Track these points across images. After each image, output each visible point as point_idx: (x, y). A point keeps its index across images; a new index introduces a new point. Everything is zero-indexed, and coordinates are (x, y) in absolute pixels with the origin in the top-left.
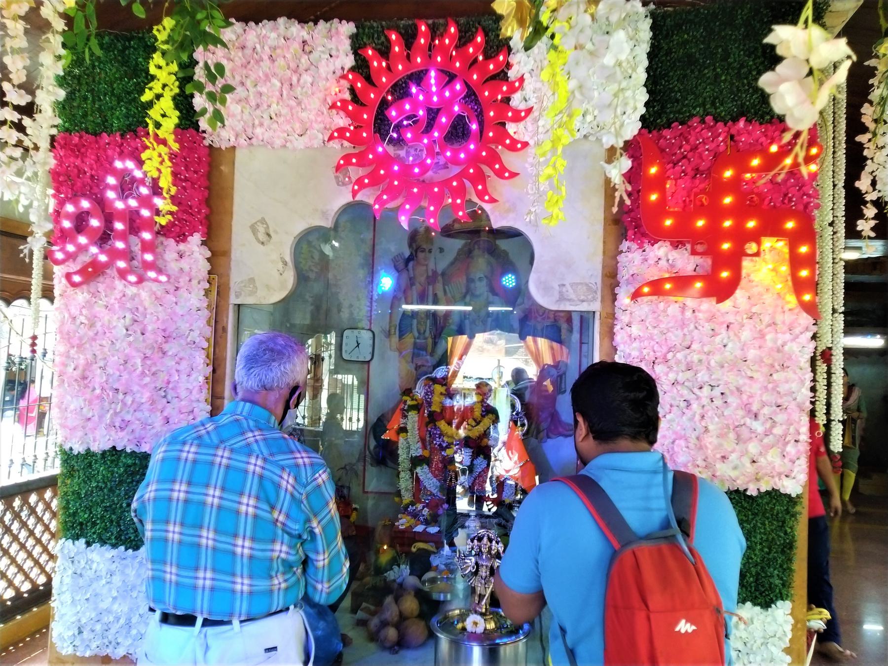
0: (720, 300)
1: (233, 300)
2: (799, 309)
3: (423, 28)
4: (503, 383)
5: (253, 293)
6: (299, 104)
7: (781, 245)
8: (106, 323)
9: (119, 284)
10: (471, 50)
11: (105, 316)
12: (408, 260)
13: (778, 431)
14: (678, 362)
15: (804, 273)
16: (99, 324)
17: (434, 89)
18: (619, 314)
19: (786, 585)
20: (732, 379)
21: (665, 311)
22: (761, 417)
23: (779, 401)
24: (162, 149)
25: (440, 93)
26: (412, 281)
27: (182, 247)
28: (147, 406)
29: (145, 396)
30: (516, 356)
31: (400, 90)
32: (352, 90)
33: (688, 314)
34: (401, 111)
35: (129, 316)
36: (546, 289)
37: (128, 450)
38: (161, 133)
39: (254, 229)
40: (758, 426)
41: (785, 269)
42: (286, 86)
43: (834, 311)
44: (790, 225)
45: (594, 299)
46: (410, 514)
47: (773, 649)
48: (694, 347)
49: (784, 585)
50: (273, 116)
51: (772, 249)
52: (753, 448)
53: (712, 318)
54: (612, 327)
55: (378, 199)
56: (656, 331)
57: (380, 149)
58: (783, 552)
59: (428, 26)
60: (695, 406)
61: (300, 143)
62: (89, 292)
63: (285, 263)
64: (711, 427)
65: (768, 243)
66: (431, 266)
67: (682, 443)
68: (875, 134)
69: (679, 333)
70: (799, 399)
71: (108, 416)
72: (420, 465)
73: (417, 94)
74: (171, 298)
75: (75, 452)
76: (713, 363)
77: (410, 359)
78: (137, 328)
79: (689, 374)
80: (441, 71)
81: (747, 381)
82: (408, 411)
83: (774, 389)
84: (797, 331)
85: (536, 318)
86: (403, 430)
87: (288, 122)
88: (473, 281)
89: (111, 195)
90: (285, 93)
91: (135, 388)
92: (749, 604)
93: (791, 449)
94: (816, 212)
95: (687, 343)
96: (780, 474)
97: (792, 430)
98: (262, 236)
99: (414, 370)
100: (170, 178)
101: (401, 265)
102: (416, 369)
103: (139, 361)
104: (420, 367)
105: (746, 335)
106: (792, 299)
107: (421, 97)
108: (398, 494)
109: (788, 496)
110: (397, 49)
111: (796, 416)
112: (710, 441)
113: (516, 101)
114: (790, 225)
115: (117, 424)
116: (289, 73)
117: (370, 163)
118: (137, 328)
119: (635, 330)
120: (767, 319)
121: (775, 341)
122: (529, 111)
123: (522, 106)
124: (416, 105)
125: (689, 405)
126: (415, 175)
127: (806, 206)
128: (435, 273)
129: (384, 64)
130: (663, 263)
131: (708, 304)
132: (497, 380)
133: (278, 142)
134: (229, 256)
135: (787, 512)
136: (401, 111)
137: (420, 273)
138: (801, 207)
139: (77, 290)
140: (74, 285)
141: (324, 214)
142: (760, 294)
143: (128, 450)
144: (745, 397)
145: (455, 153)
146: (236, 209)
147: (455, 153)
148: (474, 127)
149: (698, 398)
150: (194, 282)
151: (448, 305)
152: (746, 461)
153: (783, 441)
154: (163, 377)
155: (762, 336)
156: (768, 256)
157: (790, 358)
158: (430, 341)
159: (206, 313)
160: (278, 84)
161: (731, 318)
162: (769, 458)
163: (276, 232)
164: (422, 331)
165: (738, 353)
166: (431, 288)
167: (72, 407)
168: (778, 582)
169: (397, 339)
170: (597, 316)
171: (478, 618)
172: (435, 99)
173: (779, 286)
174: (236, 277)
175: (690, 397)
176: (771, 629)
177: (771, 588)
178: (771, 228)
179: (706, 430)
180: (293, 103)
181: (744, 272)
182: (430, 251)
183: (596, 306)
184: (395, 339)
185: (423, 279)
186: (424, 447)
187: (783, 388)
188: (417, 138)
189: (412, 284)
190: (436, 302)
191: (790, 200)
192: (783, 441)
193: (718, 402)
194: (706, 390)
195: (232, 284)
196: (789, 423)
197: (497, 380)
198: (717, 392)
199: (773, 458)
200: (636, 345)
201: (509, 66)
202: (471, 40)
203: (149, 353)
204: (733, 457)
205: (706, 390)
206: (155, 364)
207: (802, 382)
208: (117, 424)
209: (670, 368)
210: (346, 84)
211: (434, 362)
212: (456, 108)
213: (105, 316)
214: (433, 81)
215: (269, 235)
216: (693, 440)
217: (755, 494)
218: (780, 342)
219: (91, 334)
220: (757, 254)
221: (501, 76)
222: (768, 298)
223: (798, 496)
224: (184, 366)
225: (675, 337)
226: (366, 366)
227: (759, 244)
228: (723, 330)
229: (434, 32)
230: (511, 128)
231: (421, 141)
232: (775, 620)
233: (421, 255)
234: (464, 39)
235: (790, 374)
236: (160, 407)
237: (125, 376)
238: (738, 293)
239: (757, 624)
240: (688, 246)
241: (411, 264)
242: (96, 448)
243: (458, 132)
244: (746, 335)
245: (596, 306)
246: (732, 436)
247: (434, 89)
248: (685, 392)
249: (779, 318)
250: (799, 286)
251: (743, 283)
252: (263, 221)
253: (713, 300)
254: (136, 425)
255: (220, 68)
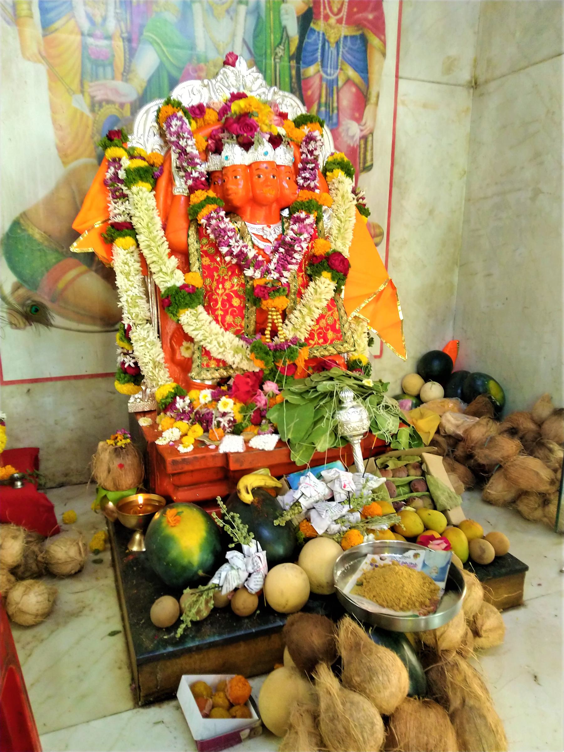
46: (182, 415)
72: (189, 305)
77: (75, 85)
82: (128, 182)
85: (327, 18)
86: (126, 228)
99: (87, 111)
102: (93, 110)
104: (100, 104)
108: (135, 375)
146: (36, 716)
158: (119, 45)
164: (98, 20)
169: (39, 31)
186: (186, 267)
211: (133, 96)
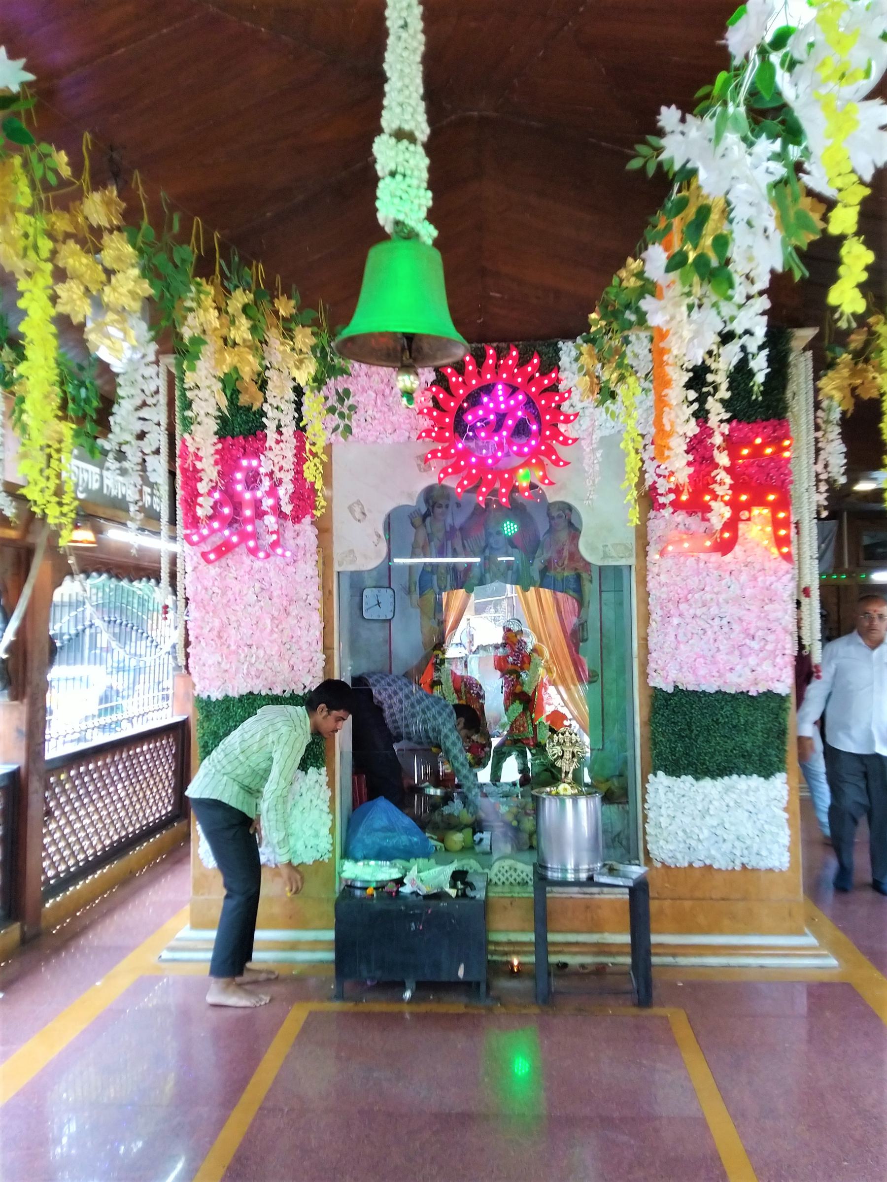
0: (724, 554)
1: (337, 568)
2: (780, 559)
3: (491, 352)
4: (474, 649)
5: (353, 561)
6: (390, 410)
7: (766, 512)
8: (237, 591)
9: (247, 560)
10: (530, 369)
11: (236, 586)
12: (424, 517)
13: (769, 647)
14: (696, 601)
15: (782, 532)
16: (230, 593)
17: (501, 399)
18: (650, 566)
19: (782, 761)
20: (732, 611)
21: (684, 563)
22: (757, 638)
23: (770, 626)
24: (317, 460)
25: (506, 401)
26: (430, 537)
27: (297, 527)
28: (276, 657)
29: (274, 650)
30: (485, 615)
31: (474, 399)
32: (435, 399)
33: (702, 565)
34: (475, 416)
35: (258, 585)
36: (592, 549)
37: (263, 693)
38: (314, 449)
39: (351, 509)
40: (755, 645)
41: (769, 529)
42: (380, 396)
43: (811, 557)
44: (771, 497)
45: (630, 556)
47: (775, 809)
48: (707, 589)
49: (780, 761)
50: (369, 419)
51: (760, 514)
52: (752, 661)
53: (718, 568)
54: (645, 576)
55: (460, 485)
56: (679, 579)
57: (460, 446)
58: (778, 737)
59: (494, 349)
60: (709, 632)
61: (389, 440)
62: (220, 567)
63: (379, 536)
64: (721, 648)
65: (756, 511)
66: (449, 520)
67: (702, 660)
68: (825, 432)
69: (696, 579)
70: (784, 623)
71: (245, 667)
73: (488, 403)
74: (291, 569)
75: (214, 699)
76: (721, 600)
77: (432, 616)
78: (266, 595)
79: (704, 609)
80: (506, 385)
81: (745, 612)
83: (765, 617)
84: (780, 574)
85: (555, 569)
87: (380, 424)
88: (491, 534)
89: (239, 487)
90: (379, 402)
91: (266, 643)
92: (755, 776)
93: (779, 660)
94: (791, 487)
95: (702, 587)
96: (772, 679)
97: (779, 646)
98: (358, 515)
100: (321, 482)
101: (418, 521)
103: (268, 622)
105: (744, 578)
106: (774, 550)
107: (491, 405)
109: (779, 695)
110: (470, 368)
111: (782, 636)
112: (721, 657)
113: (565, 407)
114: (771, 497)
115: (253, 673)
116: (382, 386)
117: (453, 456)
118: (266, 595)
119: (663, 578)
120: (758, 566)
121: (764, 582)
122: (576, 415)
123: (570, 411)
124: (488, 411)
125: (705, 633)
126: (489, 465)
127: (783, 481)
128: (452, 527)
129: (460, 379)
130: (681, 527)
131: (716, 557)
132: (467, 645)
133: (371, 439)
134: (331, 533)
135: (780, 707)
136: (475, 416)
137: (438, 528)
138: (780, 484)
139: (210, 566)
140: (209, 561)
141: (410, 495)
142: (753, 548)
143: (263, 693)
144: (745, 624)
145: (521, 447)
147: (521, 447)
148: (534, 427)
149: (712, 626)
150: (308, 555)
151: (467, 556)
152: (747, 671)
153: (773, 654)
154: (287, 632)
155: (755, 578)
156: (757, 520)
157: (776, 594)
159: (318, 580)
160: (374, 395)
161: (732, 567)
162: (764, 668)
163: (370, 511)
165: (739, 592)
166: (449, 543)
167: (210, 662)
168: (776, 759)
170: (633, 568)
171: (567, 786)
172: (503, 406)
173: (766, 542)
174: (338, 550)
175: (706, 626)
176: (772, 794)
177: (771, 765)
178: (758, 500)
179: (718, 650)
180: (385, 409)
181: (740, 533)
182: (447, 506)
183: (632, 561)
184: (416, 596)
185: (440, 535)
187: (772, 616)
188: (489, 437)
189: (430, 541)
190: (455, 554)
191: (771, 478)
192: (773, 654)
193: (726, 629)
194: (717, 620)
195: (335, 555)
196: (777, 641)
197: (467, 645)
198: (725, 621)
199: (766, 668)
200: (664, 589)
201: (558, 380)
202: (528, 361)
203: (276, 614)
204: (738, 668)
205: (717, 620)
206: (281, 622)
207: (786, 611)
208: (253, 673)
209: (690, 605)
210: (429, 395)
212: (520, 413)
213: (236, 586)
214: (500, 393)
215: (364, 514)
216: (709, 658)
217: (755, 694)
218: (768, 583)
219: (225, 601)
220: (749, 519)
221: (553, 388)
222: (759, 551)
223: (788, 696)
224: (303, 623)
225: (693, 583)
226: (387, 625)
227: (750, 512)
228: (727, 575)
229: (499, 355)
230: (562, 428)
231: (492, 438)
232: (775, 787)
233: (438, 511)
234: (523, 361)
235: (776, 606)
236: (287, 657)
237: (257, 634)
238: (737, 548)
239: (762, 791)
240: (700, 514)
241: (428, 520)
242: (234, 693)
243: (521, 429)
244: (744, 578)
245: (632, 561)
246: (737, 652)
247: (501, 399)
248: (701, 623)
249: (767, 565)
250: (781, 542)
251: (740, 540)
252: (358, 502)
253: (719, 554)
254: (269, 673)
255: (347, 392)
